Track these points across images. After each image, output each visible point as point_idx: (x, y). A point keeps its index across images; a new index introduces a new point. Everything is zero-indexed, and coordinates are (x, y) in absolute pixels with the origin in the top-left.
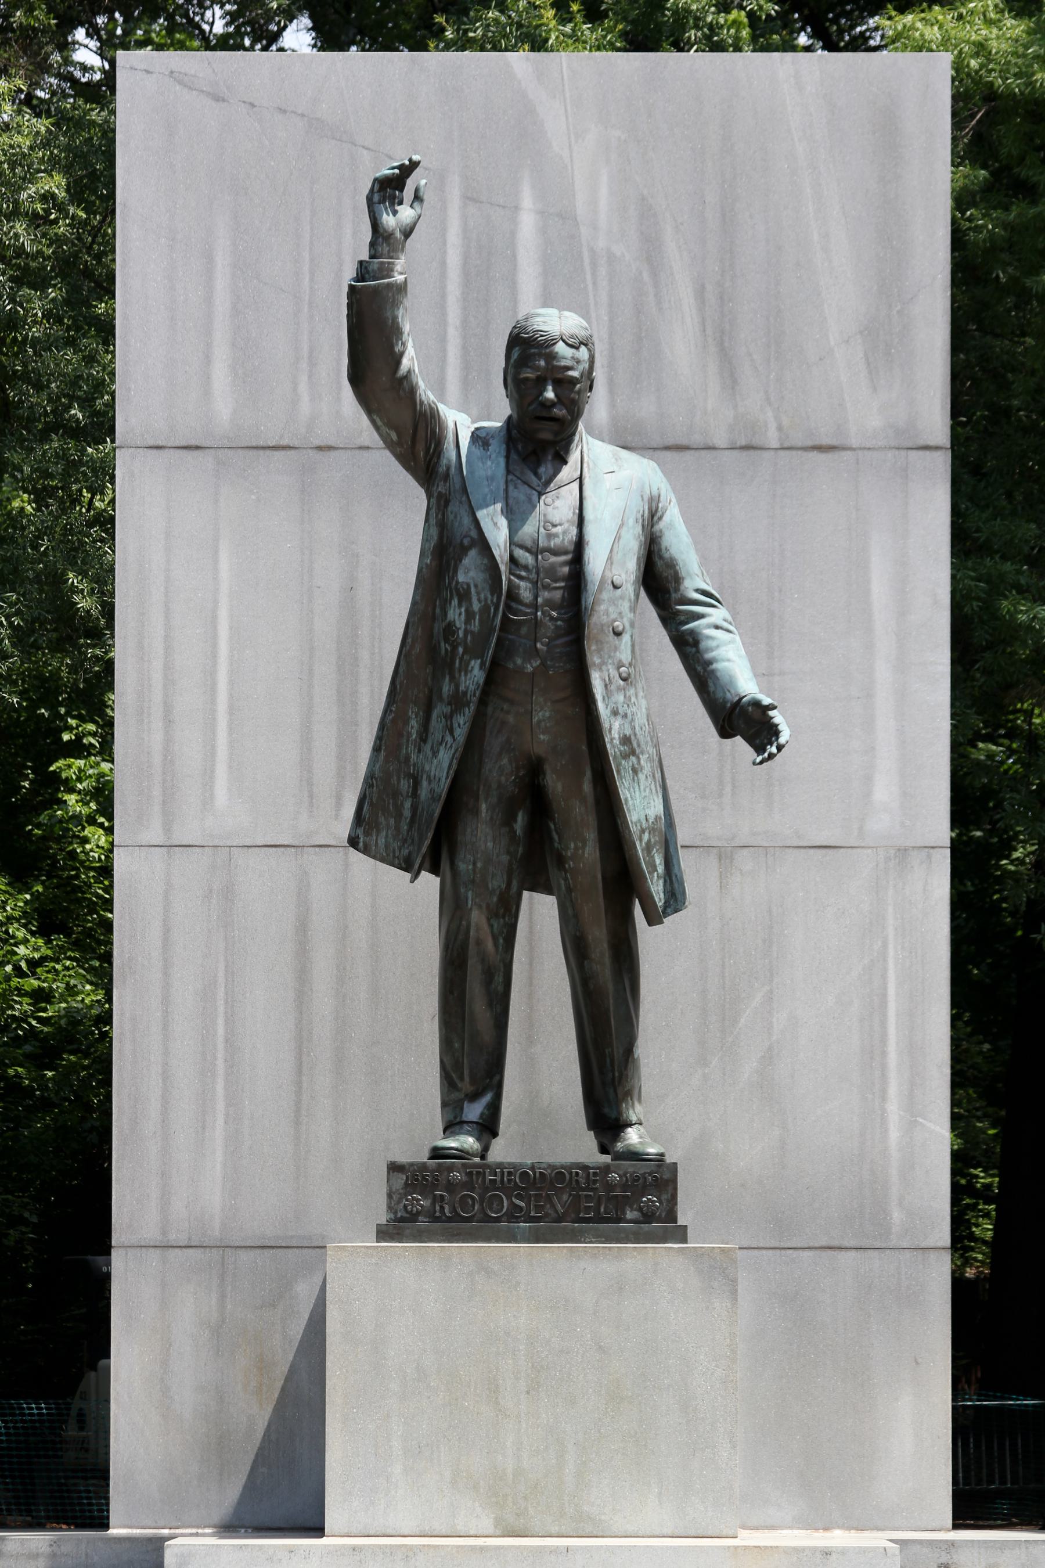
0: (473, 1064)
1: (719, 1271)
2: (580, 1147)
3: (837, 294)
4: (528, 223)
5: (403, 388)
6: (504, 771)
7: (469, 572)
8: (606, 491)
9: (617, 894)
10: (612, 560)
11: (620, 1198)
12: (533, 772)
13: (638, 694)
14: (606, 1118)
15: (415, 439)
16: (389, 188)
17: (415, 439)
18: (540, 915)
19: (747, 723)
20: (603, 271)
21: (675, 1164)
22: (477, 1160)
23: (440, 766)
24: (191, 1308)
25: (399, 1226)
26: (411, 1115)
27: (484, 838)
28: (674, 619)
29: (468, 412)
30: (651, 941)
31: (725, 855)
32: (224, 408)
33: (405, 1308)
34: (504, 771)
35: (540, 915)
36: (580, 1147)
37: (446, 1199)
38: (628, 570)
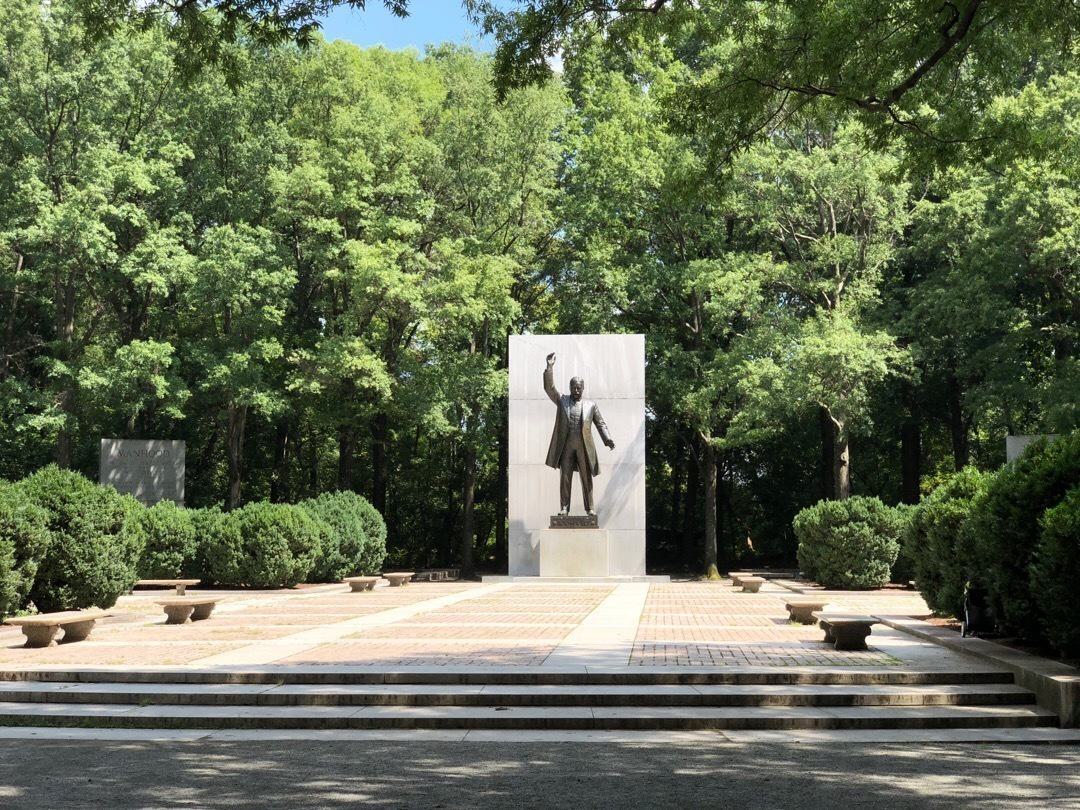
0: (566, 500)
2: (585, 514)
3: (143, 598)
4: (576, 362)
5: (553, 389)
6: (571, 451)
8: (584, 407)
9: (590, 471)
11: (589, 522)
12: (575, 454)
14: (588, 508)
16: (550, 357)
18: (576, 477)
21: (649, 572)
25: (553, 526)
26: (556, 508)
27: (567, 463)
28: (381, 423)
29: (564, 390)
30: (595, 479)
33: (552, 542)
34: (571, 451)
35: (576, 477)
36: (585, 514)
37: (559, 522)
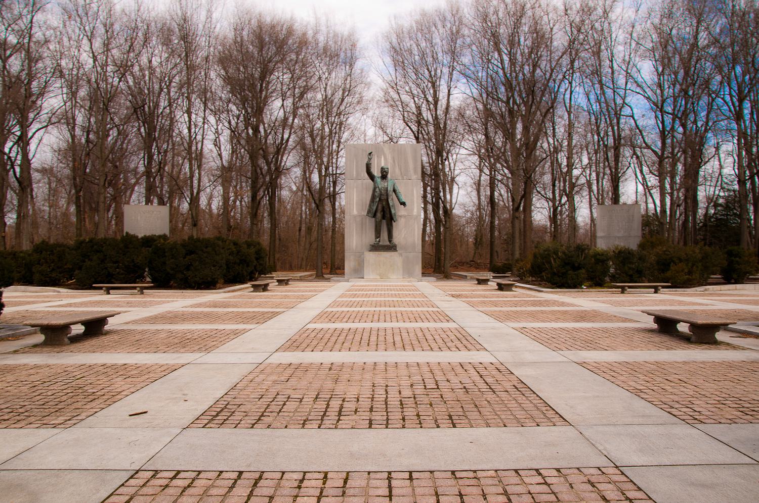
0: (378, 234)
1: (401, 255)
2: (388, 243)
7: (377, 190)
10: (390, 189)
11: (391, 248)
13: (393, 201)
14: (390, 241)
15: (372, 177)
16: (370, 154)
17: (372, 177)
19: (403, 204)
20: (536, 413)
22: (474, 48)
23: (375, 208)
24: (352, 258)
27: (379, 215)
31: (401, 216)
32: (207, 137)
33: (371, 257)
36: (388, 243)
37: (375, 248)
38: (392, 190)
